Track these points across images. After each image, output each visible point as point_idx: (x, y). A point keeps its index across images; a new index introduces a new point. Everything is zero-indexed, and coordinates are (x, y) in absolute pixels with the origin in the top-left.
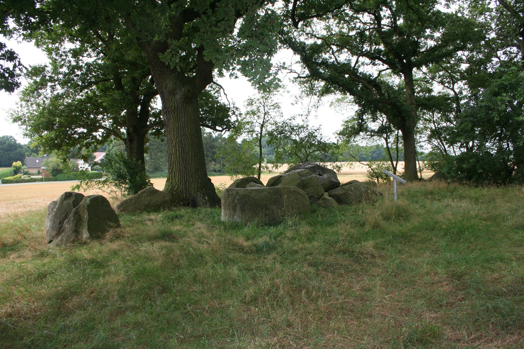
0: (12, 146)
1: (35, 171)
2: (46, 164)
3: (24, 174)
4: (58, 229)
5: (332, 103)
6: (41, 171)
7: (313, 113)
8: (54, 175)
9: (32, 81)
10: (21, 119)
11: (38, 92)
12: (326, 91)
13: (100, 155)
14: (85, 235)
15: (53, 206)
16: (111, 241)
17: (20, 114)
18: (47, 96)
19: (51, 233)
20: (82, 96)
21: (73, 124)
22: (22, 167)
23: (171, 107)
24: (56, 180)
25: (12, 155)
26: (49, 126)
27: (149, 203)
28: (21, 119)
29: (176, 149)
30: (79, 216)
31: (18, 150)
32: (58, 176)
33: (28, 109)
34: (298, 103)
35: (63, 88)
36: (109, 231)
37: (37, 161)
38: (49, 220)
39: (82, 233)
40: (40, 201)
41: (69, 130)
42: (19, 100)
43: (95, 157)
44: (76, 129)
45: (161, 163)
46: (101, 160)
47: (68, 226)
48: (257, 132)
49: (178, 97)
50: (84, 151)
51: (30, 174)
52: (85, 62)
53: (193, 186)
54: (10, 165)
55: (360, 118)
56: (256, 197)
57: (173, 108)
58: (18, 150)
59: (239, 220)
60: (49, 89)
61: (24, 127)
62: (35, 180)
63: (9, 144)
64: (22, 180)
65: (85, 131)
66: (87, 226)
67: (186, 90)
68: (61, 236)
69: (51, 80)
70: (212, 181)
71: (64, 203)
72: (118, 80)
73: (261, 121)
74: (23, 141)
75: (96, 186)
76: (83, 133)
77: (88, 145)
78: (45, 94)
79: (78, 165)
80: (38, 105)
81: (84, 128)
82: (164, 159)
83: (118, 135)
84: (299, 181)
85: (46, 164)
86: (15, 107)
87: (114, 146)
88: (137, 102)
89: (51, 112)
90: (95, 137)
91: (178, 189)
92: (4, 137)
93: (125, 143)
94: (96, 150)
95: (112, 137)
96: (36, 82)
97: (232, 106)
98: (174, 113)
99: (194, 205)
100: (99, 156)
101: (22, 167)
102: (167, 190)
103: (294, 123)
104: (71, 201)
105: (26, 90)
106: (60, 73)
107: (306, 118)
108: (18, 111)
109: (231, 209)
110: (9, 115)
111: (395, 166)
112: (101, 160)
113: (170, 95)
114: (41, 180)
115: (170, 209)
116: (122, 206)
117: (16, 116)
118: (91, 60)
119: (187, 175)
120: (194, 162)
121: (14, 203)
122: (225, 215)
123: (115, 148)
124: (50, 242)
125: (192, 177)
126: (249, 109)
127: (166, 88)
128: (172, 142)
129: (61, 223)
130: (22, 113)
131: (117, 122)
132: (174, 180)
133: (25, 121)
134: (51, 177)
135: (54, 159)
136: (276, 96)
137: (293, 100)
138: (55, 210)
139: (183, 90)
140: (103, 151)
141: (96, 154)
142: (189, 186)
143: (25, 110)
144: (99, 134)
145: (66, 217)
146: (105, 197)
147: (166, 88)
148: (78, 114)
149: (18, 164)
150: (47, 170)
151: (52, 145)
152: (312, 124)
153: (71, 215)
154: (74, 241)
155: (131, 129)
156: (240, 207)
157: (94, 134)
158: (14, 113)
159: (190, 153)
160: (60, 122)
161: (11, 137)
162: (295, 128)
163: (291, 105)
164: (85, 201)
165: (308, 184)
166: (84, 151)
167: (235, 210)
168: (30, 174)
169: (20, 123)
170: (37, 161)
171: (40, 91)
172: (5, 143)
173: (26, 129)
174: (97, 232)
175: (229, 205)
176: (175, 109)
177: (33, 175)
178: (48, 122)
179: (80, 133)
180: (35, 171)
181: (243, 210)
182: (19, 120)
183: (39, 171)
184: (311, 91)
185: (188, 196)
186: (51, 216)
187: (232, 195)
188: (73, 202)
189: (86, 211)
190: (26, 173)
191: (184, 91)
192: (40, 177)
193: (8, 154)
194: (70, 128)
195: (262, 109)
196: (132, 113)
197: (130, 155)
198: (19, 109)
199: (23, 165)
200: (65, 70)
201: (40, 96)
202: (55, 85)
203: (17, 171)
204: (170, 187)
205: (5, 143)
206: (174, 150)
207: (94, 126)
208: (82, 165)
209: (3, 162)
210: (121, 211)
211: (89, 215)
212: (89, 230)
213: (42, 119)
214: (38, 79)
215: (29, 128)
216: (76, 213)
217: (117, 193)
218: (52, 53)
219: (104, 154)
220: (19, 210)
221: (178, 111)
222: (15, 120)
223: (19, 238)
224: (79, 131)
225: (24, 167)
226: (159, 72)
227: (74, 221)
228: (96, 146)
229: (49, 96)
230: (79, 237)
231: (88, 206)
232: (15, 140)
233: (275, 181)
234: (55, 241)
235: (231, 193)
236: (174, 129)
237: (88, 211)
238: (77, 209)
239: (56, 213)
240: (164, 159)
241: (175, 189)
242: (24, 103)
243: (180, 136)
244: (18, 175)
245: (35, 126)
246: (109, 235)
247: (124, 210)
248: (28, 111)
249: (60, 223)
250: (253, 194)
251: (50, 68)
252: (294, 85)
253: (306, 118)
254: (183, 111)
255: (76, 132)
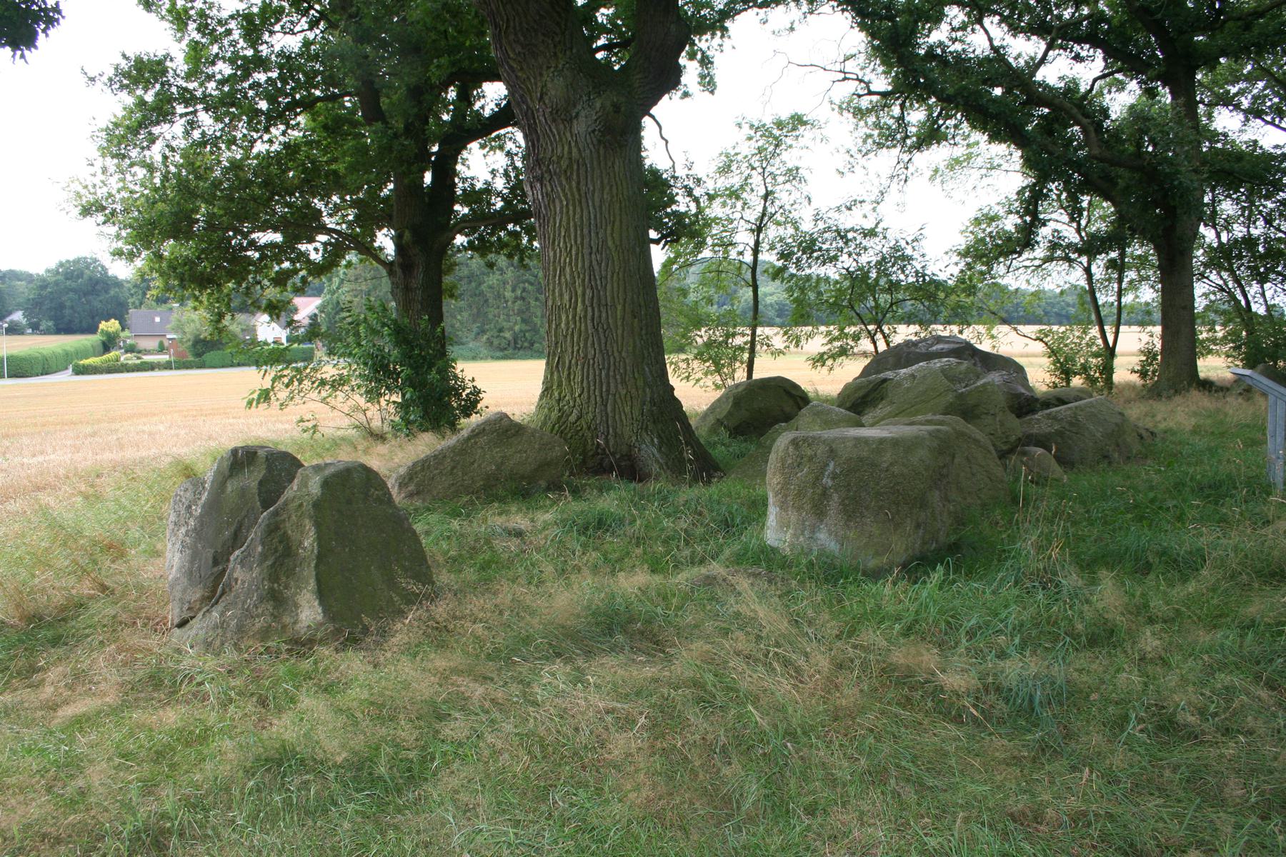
0: (97, 282)
1: (152, 344)
2: (179, 328)
3: (127, 352)
4: (211, 581)
5: (936, 171)
6: (166, 344)
7: (893, 196)
8: (199, 355)
9: (130, 100)
10: (104, 208)
11: (150, 133)
12: (931, 135)
13: (307, 305)
14: (309, 612)
15: (189, 495)
16: (412, 651)
17: (101, 192)
18: (174, 144)
19: (184, 591)
20: (271, 141)
21: (247, 219)
22: (122, 334)
23: (560, 158)
24: (202, 366)
25: (97, 304)
26: (179, 226)
27: (498, 468)
28: (104, 208)
29: (573, 295)
30: (285, 539)
31: (112, 293)
32: (208, 357)
33: (123, 180)
34: (857, 169)
35: (218, 119)
36: (402, 614)
37: (157, 319)
38: (178, 546)
39: (297, 606)
40: (161, 428)
41: (235, 237)
42: (96, 154)
43: (296, 310)
44: (254, 236)
45: (458, 325)
46: (311, 318)
47: (244, 574)
48: (740, 248)
49: (580, 127)
50: (272, 293)
51: (139, 352)
52: (277, 48)
53: (627, 409)
54: (92, 330)
55: (1027, 212)
56: (896, 469)
57: (564, 164)
58: (112, 293)
59: (833, 546)
60: (178, 127)
61: (113, 230)
62: (152, 367)
63: (90, 279)
64: (123, 365)
65: (277, 237)
66: (312, 584)
67: (608, 103)
68: (220, 607)
69: (187, 98)
70: (676, 393)
71: (229, 489)
72: (370, 96)
73: (752, 215)
74: (123, 271)
75: (314, 395)
76: (272, 245)
77: (281, 280)
78: (168, 137)
79: (253, 330)
80: (151, 168)
81: (275, 230)
82: (465, 314)
83: (370, 251)
84: (950, 397)
85: (179, 328)
86: (85, 174)
87: (342, 281)
88: (422, 159)
89: (182, 186)
90: (303, 256)
91: (579, 418)
92: (77, 261)
93: (391, 273)
94: (300, 291)
95: (352, 256)
96: (142, 103)
97: (681, 172)
98: (569, 179)
99: (632, 471)
100: (306, 307)
101: (122, 334)
102: (544, 423)
103: (847, 221)
104: (251, 479)
105: (116, 125)
106: (210, 77)
107: (874, 209)
108: (94, 186)
109: (807, 507)
110: (72, 195)
111: (1110, 339)
112: (311, 318)
113: (554, 120)
114: (167, 366)
115: (576, 492)
116: (411, 479)
117: (91, 198)
118: (293, 43)
119: (608, 375)
120: (619, 330)
121: (94, 434)
122: (784, 525)
123: (345, 288)
124: (182, 624)
125: (623, 382)
126: (723, 183)
127: (541, 98)
128: (563, 270)
129: (220, 559)
130: (105, 190)
131: (370, 217)
132: (566, 391)
133: (113, 213)
134: (191, 358)
135: (192, 317)
136: (793, 151)
137: (841, 161)
138: (197, 510)
139: (598, 105)
140: (314, 295)
141: (298, 301)
142: (614, 410)
143: (114, 183)
144: (314, 250)
145: (237, 540)
146: (375, 468)
147: (541, 98)
148: (255, 192)
149: (112, 325)
150: (181, 341)
151: (191, 278)
152: (898, 223)
153: (255, 534)
154: (265, 634)
155: (407, 235)
156: (842, 503)
157: (303, 247)
158: (83, 192)
159: (619, 307)
160: (210, 217)
161: (95, 260)
162: (850, 235)
163: (839, 176)
164: (304, 484)
165: (977, 405)
166: (272, 293)
167: (819, 511)
168: (139, 352)
169: (101, 218)
170: (157, 319)
171: (156, 130)
172: (81, 275)
173: (118, 237)
174: (356, 616)
175: (800, 494)
176: (570, 166)
177: (148, 352)
178: (175, 214)
179: (266, 246)
180: (152, 344)
181: (852, 511)
182: (97, 211)
183: (161, 344)
184: (891, 137)
185: (611, 443)
186: (183, 530)
187: (811, 459)
188: (261, 483)
189: (308, 524)
190: (131, 349)
191: (603, 106)
192: (164, 358)
193: (89, 302)
194: (238, 231)
195: (756, 179)
196: (410, 188)
197: (405, 305)
198: (97, 181)
199: (123, 329)
200: (224, 69)
201: (153, 142)
202: (195, 112)
203: (109, 344)
204: (554, 415)
205: (81, 275)
206: (566, 297)
207: (304, 224)
208: (268, 331)
209: (77, 321)
210: (411, 495)
211: (319, 538)
212: (323, 594)
213: (160, 206)
214: (149, 97)
215: (124, 233)
216: (273, 528)
217: (369, 414)
218: (187, 25)
219: (317, 302)
220: (108, 456)
221: (582, 171)
222: (86, 211)
223: (86, 588)
224: (262, 242)
225: (127, 333)
226: (519, 49)
227: (264, 557)
228: (304, 280)
229: (181, 143)
230: (287, 619)
231: (316, 505)
232: (103, 267)
233: (865, 397)
234: (198, 627)
235: (809, 452)
236: (567, 230)
237: (318, 525)
238: (276, 514)
239: (201, 519)
240: (465, 314)
241: (573, 418)
242: (111, 163)
243: (586, 251)
244: (112, 354)
245: (140, 227)
246: (404, 631)
247: (418, 493)
248: (121, 184)
249: (216, 562)
250: (888, 457)
251: (179, 63)
252: (842, 119)
253: (874, 209)
254: (597, 172)
255: (252, 244)
